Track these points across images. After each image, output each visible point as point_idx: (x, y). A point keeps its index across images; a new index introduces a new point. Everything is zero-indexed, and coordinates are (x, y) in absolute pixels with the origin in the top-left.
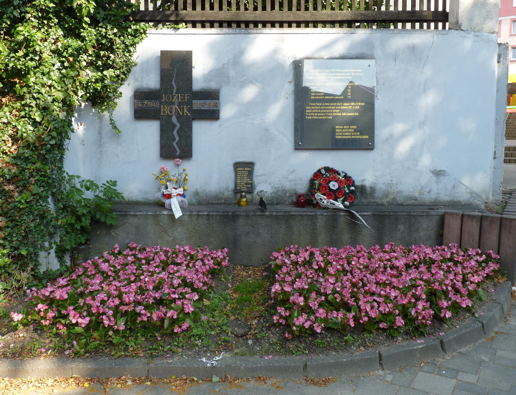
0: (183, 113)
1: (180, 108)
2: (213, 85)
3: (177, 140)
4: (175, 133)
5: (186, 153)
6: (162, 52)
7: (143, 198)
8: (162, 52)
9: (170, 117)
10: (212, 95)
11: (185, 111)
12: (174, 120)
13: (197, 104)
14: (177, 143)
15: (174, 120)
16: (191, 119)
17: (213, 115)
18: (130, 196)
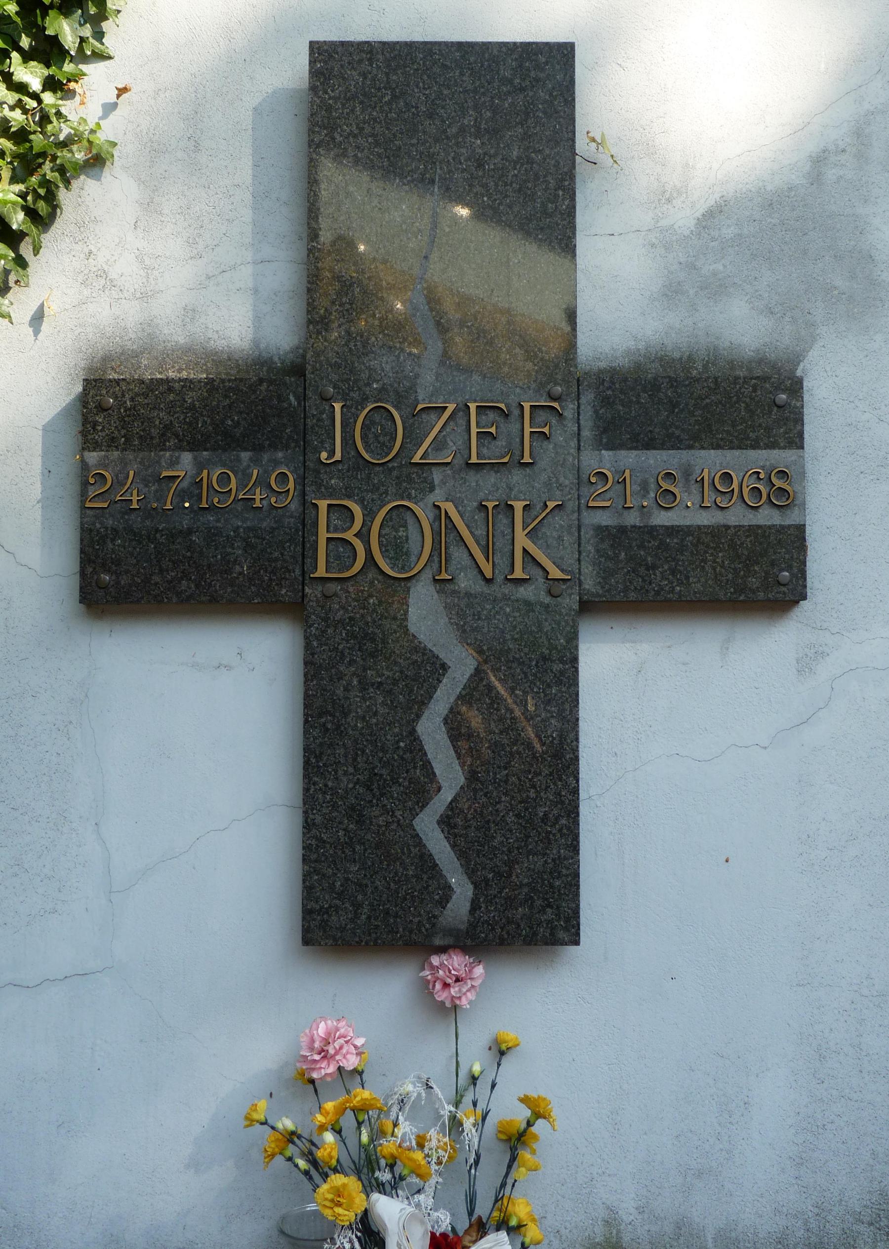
2: (740, 326)
3: (447, 796)
14: (446, 822)
17: (754, 574)
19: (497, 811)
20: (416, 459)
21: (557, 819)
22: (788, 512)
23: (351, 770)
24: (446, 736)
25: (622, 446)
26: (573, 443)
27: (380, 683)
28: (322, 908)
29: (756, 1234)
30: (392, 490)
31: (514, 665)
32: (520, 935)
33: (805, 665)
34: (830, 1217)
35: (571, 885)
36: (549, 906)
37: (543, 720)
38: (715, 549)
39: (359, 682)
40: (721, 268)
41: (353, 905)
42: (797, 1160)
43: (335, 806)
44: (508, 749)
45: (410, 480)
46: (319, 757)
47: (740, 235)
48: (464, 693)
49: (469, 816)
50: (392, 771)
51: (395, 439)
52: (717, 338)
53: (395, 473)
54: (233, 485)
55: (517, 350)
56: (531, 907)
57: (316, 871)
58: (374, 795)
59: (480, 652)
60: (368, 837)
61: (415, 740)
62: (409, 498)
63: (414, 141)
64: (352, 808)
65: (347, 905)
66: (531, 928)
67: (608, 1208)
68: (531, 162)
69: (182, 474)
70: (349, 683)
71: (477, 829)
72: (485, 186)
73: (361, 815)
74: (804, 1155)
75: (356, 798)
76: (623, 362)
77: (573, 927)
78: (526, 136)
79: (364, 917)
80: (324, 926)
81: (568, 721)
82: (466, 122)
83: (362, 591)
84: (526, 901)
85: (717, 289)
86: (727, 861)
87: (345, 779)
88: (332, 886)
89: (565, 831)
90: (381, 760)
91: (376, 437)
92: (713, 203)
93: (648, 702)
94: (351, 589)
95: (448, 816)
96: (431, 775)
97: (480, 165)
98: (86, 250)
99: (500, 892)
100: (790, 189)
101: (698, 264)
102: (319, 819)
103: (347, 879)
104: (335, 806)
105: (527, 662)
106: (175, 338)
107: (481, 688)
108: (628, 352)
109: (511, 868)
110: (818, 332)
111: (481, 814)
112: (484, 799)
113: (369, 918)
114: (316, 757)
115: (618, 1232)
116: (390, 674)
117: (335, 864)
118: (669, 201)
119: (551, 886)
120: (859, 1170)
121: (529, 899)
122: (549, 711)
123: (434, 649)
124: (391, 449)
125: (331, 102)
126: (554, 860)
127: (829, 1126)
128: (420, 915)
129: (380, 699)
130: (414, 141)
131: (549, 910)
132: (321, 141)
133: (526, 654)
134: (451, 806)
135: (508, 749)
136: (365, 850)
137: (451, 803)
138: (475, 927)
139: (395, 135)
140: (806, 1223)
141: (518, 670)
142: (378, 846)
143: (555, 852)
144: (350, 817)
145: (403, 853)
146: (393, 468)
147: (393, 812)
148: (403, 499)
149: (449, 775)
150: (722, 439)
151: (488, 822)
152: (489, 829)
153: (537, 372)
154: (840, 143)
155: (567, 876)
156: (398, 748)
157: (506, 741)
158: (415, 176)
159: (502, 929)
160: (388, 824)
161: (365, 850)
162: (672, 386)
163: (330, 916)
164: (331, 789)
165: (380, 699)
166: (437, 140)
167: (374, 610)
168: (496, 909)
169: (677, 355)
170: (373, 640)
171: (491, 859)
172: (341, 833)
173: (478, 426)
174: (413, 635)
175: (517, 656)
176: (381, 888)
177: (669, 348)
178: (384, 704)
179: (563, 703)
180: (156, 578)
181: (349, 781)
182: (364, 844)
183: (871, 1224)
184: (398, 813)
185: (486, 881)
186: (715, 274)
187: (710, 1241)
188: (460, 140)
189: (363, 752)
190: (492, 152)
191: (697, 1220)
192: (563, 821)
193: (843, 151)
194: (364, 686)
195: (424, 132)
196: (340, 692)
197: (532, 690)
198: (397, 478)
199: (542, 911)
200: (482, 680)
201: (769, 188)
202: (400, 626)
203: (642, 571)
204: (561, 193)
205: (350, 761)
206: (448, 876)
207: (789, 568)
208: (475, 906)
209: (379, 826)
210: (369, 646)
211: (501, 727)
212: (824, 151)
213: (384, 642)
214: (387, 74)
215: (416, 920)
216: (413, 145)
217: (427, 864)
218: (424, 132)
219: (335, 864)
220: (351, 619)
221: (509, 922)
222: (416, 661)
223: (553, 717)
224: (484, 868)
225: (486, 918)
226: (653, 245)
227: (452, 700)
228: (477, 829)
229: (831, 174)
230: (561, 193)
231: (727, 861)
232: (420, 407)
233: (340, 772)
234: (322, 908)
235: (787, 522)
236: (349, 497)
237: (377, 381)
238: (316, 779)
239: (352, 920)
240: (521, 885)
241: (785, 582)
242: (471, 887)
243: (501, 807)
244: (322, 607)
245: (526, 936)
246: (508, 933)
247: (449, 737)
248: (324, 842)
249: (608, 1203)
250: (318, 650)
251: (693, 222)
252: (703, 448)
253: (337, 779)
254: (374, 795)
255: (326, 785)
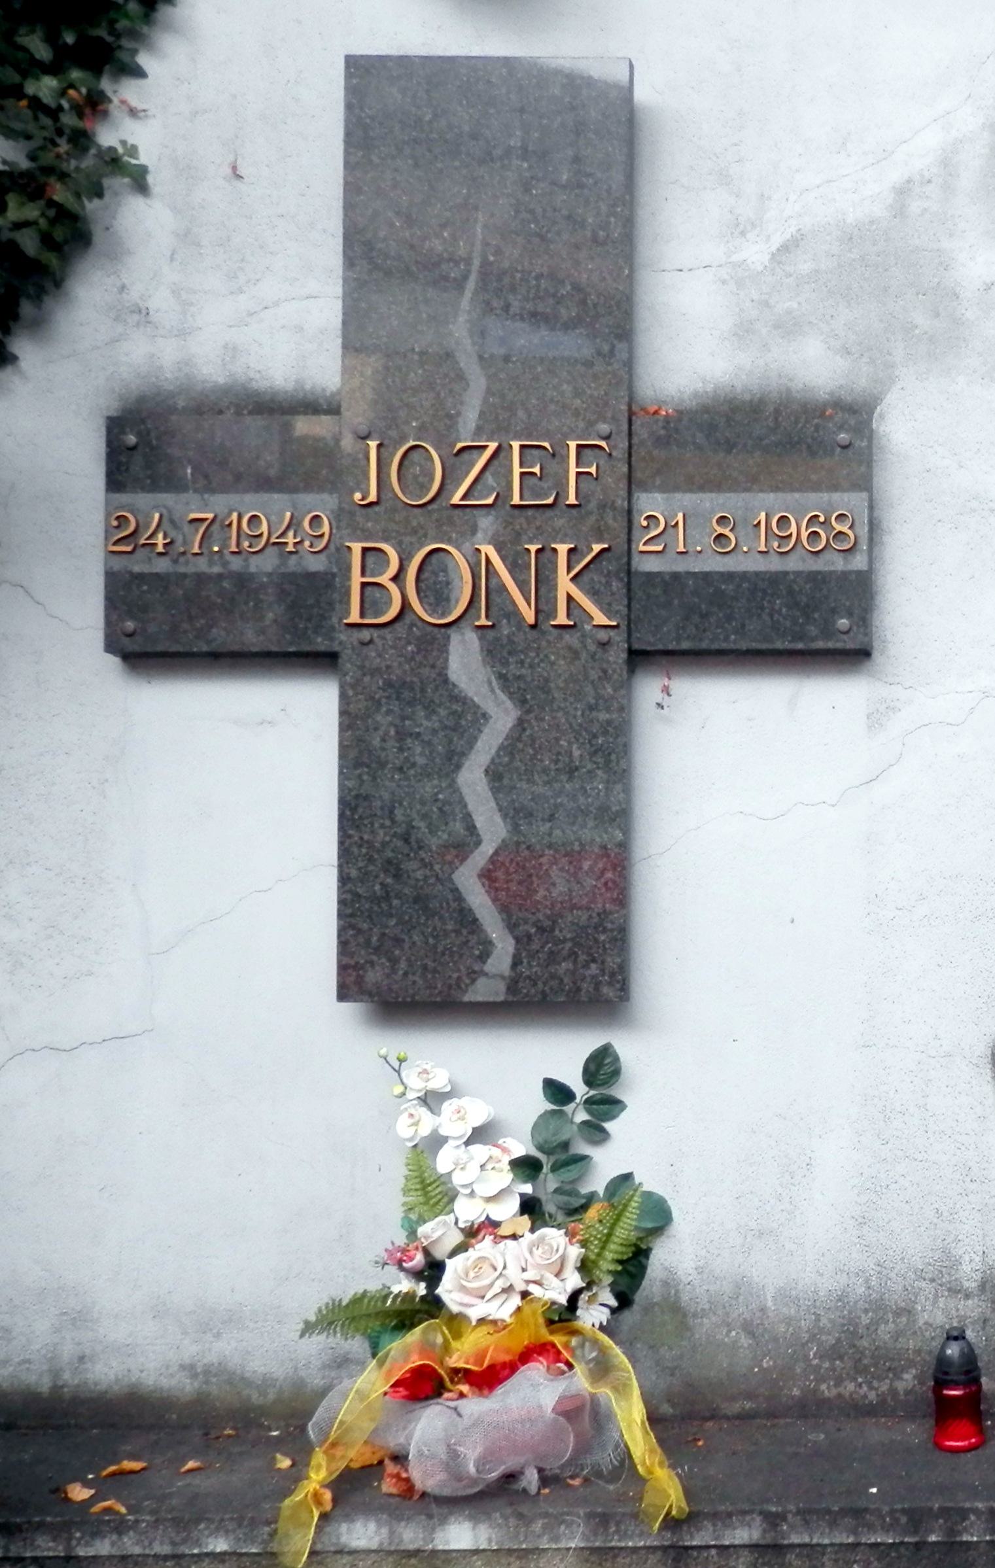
0: (544, 610)
1: (516, 566)
2: (813, 365)
3: (487, 848)
4: (472, 779)
5: (577, 961)
6: (343, 994)
7: (190, 1369)
8: (343, 994)
9: (433, 641)
10: (810, 441)
11: (564, 584)
12: (465, 664)
13: (682, 528)
14: (487, 876)
15: (465, 664)
16: (617, 656)
17: (812, 624)
18: (68, 1351)
19: (541, 864)
20: (456, 500)
21: (603, 872)
22: (850, 557)
23: (388, 823)
24: (486, 788)
25: (676, 488)
26: (623, 485)
27: (419, 734)
28: (357, 963)
29: (816, 1292)
30: (432, 532)
31: (560, 714)
32: (563, 990)
33: (875, 720)
34: (892, 1275)
35: (616, 940)
36: (594, 961)
37: (589, 772)
38: (772, 595)
39: (397, 733)
40: (795, 306)
41: (389, 960)
42: (860, 1220)
43: (371, 860)
44: (552, 801)
45: (451, 523)
46: (354, 810)
47: (817, 271)
48: (506, 743)
49: (512, 870)
50: (430, 824)
51: (432, 480)
52: (790, 380)
53: (436, 515)
54: (264, 528)
55: (565, 386)
56: (575, 962)
57: (352, 927)
58: (411, 849)
59: (523, 702)
60: (406, 891)
61: (454, 792)
62: (449, 542)
63: (457, 164)
64: (389, 862)
65: (383, 960)
66: (575, 983)
67: (666, 1269)
68: (580, 186)
69: (210, 516)
70: (386, 733)
71: (520, 883)
72: (532, 212)
73: (398, 869)
74: (867, 1215)
75: (393, 851)
76: (690, 404)
77: (618, 982)
78: (577, 159)
79: (401, 972)
80: (360, 981)
81: (615, 772)
82: (512, 143)
83: (400, 639)
84: (569, 956)
85: (789, 327)
86: (792, 921)
87: (381, 832)
88: (368, 943)
89: (610, 884)
90: (418, 812)
91: (416, 477)
92: (789, 236)
93: (719, 761)
94: (389, 636)
95: (489, 871)
96: (471, 828)
97: (527, 190)
98: (119, 284)
99: (542, 947)
100: (872, 222)
101: (772, 302)
102: (354, 873)
103: (384, 934)
104: (371, 860)
105: (572, 712)
106: (214, 378)
107: (524, 738)
108: (696, 395)
109: (554, 922)
110: (897, 373)
111: (524, 868)
112: (526, 853)
113: (406, 974)
114: (351, 809)
115: (677, 1291)
116: (429, 724)
117: (371, 919)
118: (743, 234)
119: (596, 941)
120: (923, 1229)
121: (573, 954)
122: (595, 763)
123: (476, 699)
124: (429, 490)
125: (368, 121)
126: (599, 914)
127: (893, 1186)
128: (459, 970)
129: (418, 750)
130: (457, 164)
131: (593, 966)
132: (358, 163)
133: (571, 704)
134: (493, 860)
135: (552, 801)
136: (402, 904)
137: (492, 857)
138: (517, 982)
139: (436, 157)
140: (867, 1281)
141: (563, 720)
142: (417, 900)
143: (600, 906)
144: (386, 871)
145: (442, 908)
146: (434, 511)
147: (432, 866)
148: (442, 542)
149: (492, 829)
150: (781, 482)
151: (530, 876)
152: (532, 883)
153: (585, 410)
154: (926, 174)
155: (612, 930)
156: (437, 800)
157: (550, 793)
158: (458, 201)
159: (545, 984)
160: (426, 877)
161: (402, 904)
162: (730, 426)
163: (366, 971)
164: (367, 842)
165: (418, 750)
166: (482, 162)
167: (413, 659)
168: (538, 965)
169: (747, 397)
170: (412, 689)
171: (533, 914)
172: (377, 887)
173: (521, 466)
174: (454, 685)
175: (562, 705)
176: (419, 943)
177: (739, 390)
178: (421, 754)
179: (610, 754)
180: (185, 626)
181: (385, 834)
182: (400, 898)
183: (933, 1280)
184: (437, 867)
185: (529, 937)
186: (789, 312)
187: (770, 1299)
188: (506, 162)
189: (401, 804)
190: (540, 175)
191: (756, 1279)
192: (609, 875)
193: (929, 182)
194: (401, 735)
195: (468, 154)
196: (376, 742)
197: (577, 740)
198: (437, 520)
199: (586, 966)
200: (524, 730)
201: (849, 221)
202: (440, 674)
203: (696, 619)
204: (612, 220)
205: (387, 812)
206: (489, 930)
207: (850, 614)
208: (516, 962)
209: (417, 880)
210: (406, 694)
211: (546, 778)
212: (908, 182)
213: (423, 690)
214: (427, 91)
215: (455, 975)
216: (456, 168)
217: (467, 920)
218: (468, 154)
219: (371, 919)
220: (388, 667)
221: (553, 976)
222: (456, 711)
223: (598, 768)
224: (526, 923)
225: (528, 973)
226: (724, 282)
227: (493, 751)
228: (520, 883)
229: (915, 207)
230: (612, 220)
231: (792, 921)
232: (459, 445)
233: (376, 825)
234: (357, 963)
235: (850, 567)
236: (386, 540)
237: (417, 419)
238: (351, 832)
239: (388, 976)
240: (564, 941)
241: (845, 629)
242: (513, 942)
243: (544, 860)
244: (358, 655)
245: (570, 991)
246: (551, 989)
247: (491, 789)
248: (359, 896)
249: (667, 1264)
250: (354, 699)
251: (768, 257)
252: (761, 491)
253: (372, 832)
254: (411, 849)
255: (361, 838)
